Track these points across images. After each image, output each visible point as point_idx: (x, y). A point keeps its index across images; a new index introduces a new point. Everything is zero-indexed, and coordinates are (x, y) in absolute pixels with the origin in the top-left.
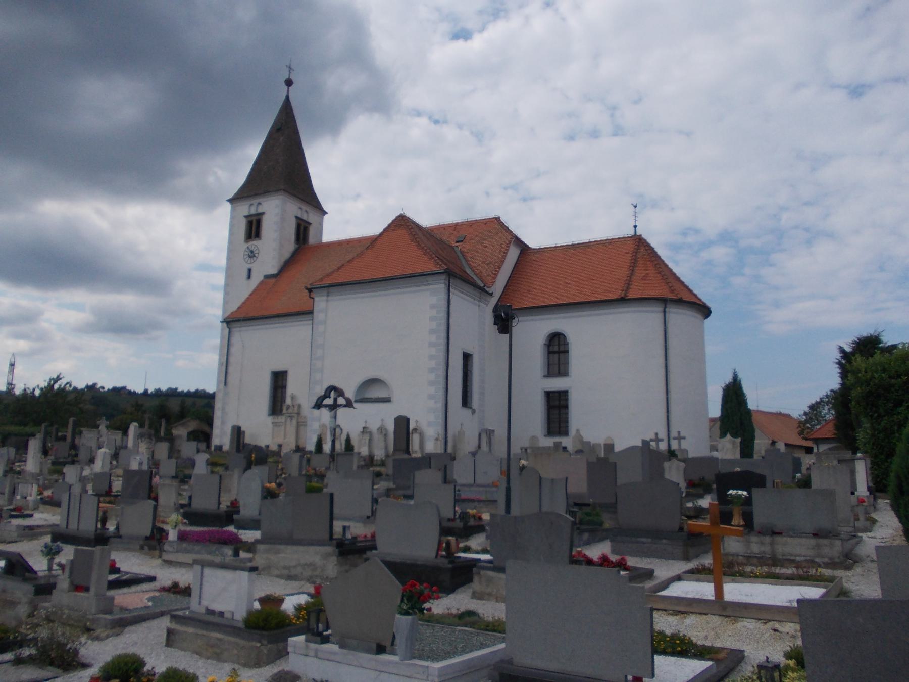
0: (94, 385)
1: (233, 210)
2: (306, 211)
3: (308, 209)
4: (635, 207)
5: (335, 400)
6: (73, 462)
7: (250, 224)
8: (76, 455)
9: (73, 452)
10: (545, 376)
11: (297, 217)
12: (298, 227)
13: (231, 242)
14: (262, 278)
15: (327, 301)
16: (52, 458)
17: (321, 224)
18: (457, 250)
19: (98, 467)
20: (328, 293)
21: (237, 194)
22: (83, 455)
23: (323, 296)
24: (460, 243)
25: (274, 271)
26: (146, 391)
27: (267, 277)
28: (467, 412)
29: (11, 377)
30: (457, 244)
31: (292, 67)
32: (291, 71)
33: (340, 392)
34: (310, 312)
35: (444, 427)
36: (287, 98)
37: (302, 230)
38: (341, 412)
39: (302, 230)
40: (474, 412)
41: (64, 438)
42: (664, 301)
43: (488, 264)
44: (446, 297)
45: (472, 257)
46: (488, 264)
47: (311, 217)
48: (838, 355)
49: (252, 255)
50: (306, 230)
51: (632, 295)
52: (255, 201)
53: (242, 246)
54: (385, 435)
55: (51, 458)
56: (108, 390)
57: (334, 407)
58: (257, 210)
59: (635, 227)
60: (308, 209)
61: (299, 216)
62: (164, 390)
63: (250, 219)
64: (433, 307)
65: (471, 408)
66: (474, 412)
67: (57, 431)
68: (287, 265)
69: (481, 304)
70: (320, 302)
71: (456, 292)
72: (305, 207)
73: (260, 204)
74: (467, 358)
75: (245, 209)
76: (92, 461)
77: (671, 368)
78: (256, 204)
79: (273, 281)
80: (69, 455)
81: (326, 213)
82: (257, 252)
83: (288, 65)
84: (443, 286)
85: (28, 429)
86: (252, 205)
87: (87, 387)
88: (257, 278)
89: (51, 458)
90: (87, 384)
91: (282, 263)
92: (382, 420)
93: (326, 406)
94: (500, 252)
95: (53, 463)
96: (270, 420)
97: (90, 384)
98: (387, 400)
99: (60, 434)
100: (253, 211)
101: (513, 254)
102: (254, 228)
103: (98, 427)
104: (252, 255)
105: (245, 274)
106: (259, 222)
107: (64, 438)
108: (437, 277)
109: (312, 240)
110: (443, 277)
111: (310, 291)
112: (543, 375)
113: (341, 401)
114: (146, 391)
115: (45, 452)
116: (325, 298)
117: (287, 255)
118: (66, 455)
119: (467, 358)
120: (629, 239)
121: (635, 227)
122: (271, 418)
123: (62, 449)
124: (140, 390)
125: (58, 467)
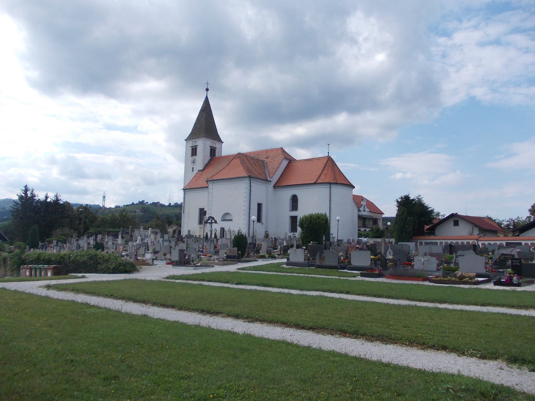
0: (143, 201)
1: (187, 143)
2: (215, 143)
3: (215, 142)
4: (329, 145)
5: (212, 221)
6: (131, 241)
7: (193, 149)
8: (132, 239)
9: (131, 238)
10: (290, 211)
11: (210, 146)
12: (211, 150)
13: (186, 157)
14: (197, 171)
15: (213, 185)
16: (125, 240)
17: (221, 147)
18: (265, 161)
19: (138, 242)
20: (213, 182)
21: (188, 137)
22: (134, 238)
23: (211, 183)
24: (266, 159)
25: (202, 169)
26: (170, 204)
27: (199, 171)
28: (260, 224)
29: (104, 203)
30: (266, 159)
31: (208, 83)
32: (208, 85)
33: (213, 218)
34: (208, 187)
35: (248, 229)
36: (207, 96)
37: (213, 151)
38: (213, 224)
39: (213, 151)
40: (263, 224)
41: (128, 233)
42: (330, 184)
43: (273, 168)
44: (250, 185)
45: (269, 165)
46: (273, 168)
47: (217, 145)
48: (396, 204)
49: (194, 162)
50: (214, 151)
51: (319, 181)
52: (194, 141)
53: (191, 159)
54: (230, 232)
55: (124, 240)
56: (150, 204)
57: (211, 223)
58: (195, 144)
59: (328, 153)
60: (215, 142)
61: (211, 145)
62: (179, 204)
63: (193, 148)
64: (245, 189)
65: (261, 222)
66: (263, 224)
67: (126, 230)
68: (206, 166)
69: (266, 185)
70: (210, 185)
71: (254, 182)
72: (214, 141)
73: (196, 141)
74: (260, 206)
75: (191, 144)
76: (136, 241)
77: (332, 208)
78: (195, 142)
79: (201, 172)
80: (130, 239)
81: (216, 148)
82: (195, 161)
83: (207, 82)
84: (248, 181)
85: (116, 230)
86: (193, 142)
87: (139, 202)
88: (196, 171)
89: (124, 240)
90: (139, 201)
91: (205, 165)
92: (229, 227)
93: (209, 223)
94: (278, 163)
95: (125, 241)
96: (199, 226)
97: (141, 201)
98: (231, 220)
99: (127, 231)
100: (194, 145)
101: (285, 163)
102: (194, 152)
103: (140, 229)
104: (194, 162)
105: (191, 170)
106: (196, 149)
107: (128, 233)
108: (246, 178)
109: (217, 155)
110: (248, 178)
111: (207, 182)
112: (289, 210)
113: (213, 221)
114: (170, 204)
115: (122, 238)
116: (212, 184)
117: (207, 162)
118: (129, 239)
119: (260, 206)
120: (326, 157)
121: (328, 153)
122: (199, 225)
123: (127, 237)
124: (167, 204)
125: (127, 242)
